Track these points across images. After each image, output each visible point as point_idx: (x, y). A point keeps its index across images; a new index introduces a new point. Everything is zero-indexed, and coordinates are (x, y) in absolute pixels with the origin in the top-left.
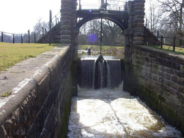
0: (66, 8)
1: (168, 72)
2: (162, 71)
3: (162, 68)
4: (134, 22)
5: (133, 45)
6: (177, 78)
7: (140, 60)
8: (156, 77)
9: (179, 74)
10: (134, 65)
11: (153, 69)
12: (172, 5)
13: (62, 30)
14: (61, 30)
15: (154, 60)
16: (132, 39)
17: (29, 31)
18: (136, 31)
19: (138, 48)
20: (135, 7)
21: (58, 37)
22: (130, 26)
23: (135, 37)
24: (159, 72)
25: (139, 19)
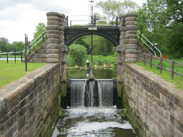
0: (52, 25)
9: (159, 103)
10: (125, 85)
16: (124, 56)
17: (26, 38)
25: (130, 35)
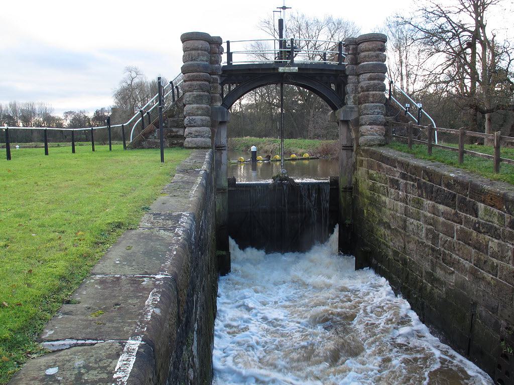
0: (196, 62)
1: (449, 220)
2: (434, 214)
3: (434, 206)
4: (359, 89)
5: (358, 145)
6: (471, 234)
7: (379, 184)
8: (418, 227)
9: (477, 225)
10: (362, 194)
11: (412, 209)
12: (450, 34)
13: (187, 117)
14: (185, 117)
15: (413, 185)
16: (357, 131)
18: (365, 112)
19: (372, 154)
20: (363, 54)
21: (181, 132)
22: (352, 100)
23: (363, 127)
24: (425, 216)
